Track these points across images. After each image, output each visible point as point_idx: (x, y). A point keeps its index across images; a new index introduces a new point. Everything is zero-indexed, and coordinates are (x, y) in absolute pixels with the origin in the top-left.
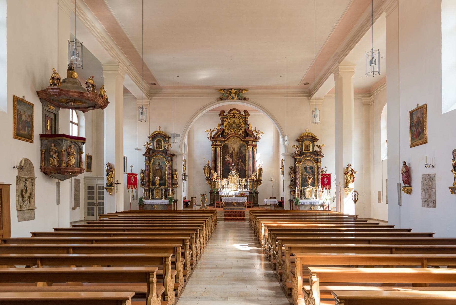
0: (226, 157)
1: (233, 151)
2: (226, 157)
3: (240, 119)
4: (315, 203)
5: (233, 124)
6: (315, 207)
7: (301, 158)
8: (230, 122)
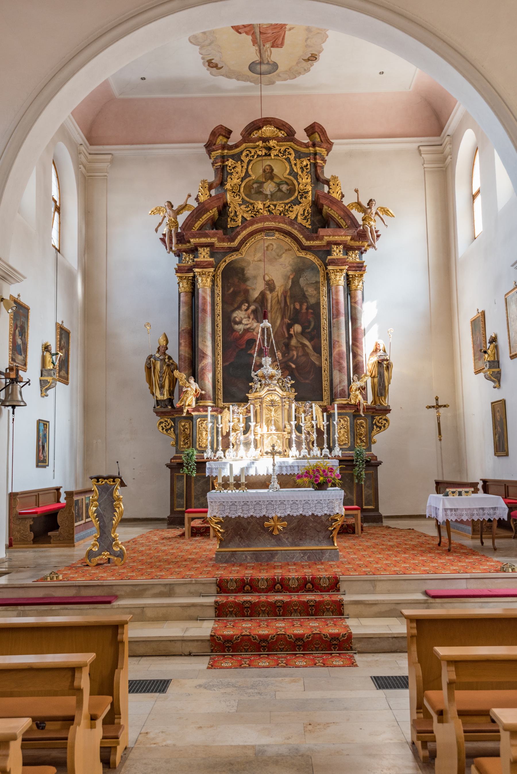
2: (239, 315)
3: (293, 162)
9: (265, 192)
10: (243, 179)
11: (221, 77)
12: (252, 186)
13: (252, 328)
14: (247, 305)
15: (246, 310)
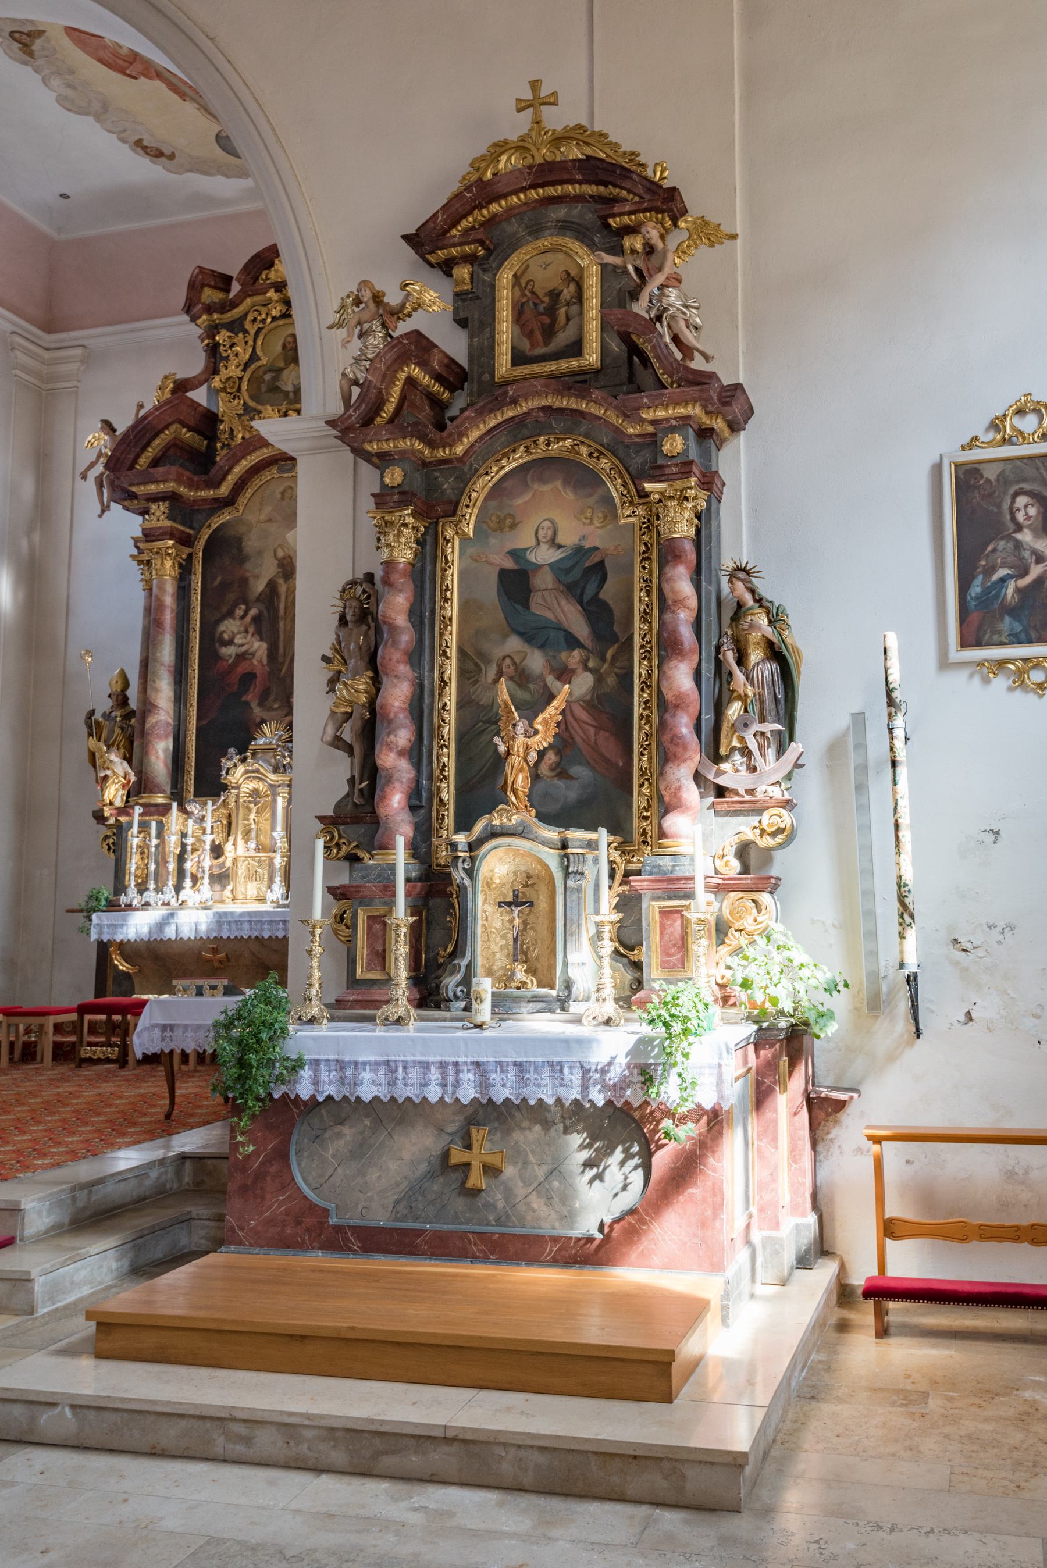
0: (229, 627)
1: (281, 581)
2: (229, 627)
4: (512, 1074)
5: (282, 364)
6: (517, 1136)
7: (459, 450)
8: (259, 359)
9: (284, 388)
10: (246, 366)
11: (190, 174)
12: (262, 377)
13: (251, 651)
14: (243, 607)
15: (242, 618)
